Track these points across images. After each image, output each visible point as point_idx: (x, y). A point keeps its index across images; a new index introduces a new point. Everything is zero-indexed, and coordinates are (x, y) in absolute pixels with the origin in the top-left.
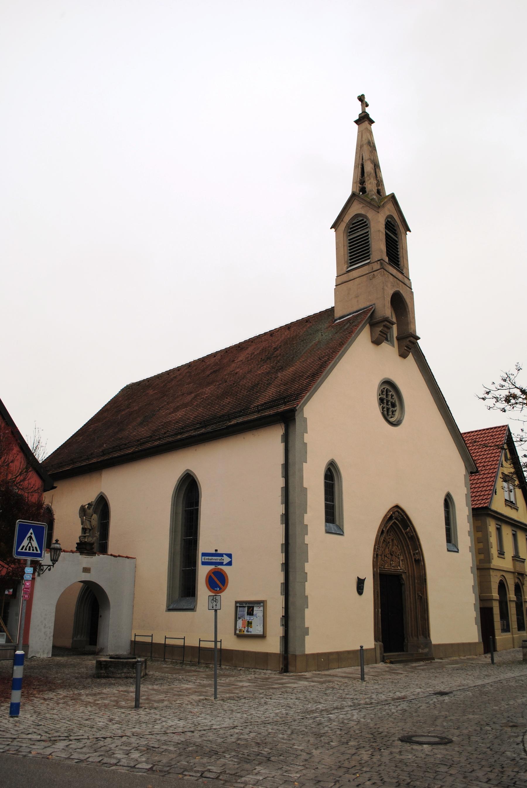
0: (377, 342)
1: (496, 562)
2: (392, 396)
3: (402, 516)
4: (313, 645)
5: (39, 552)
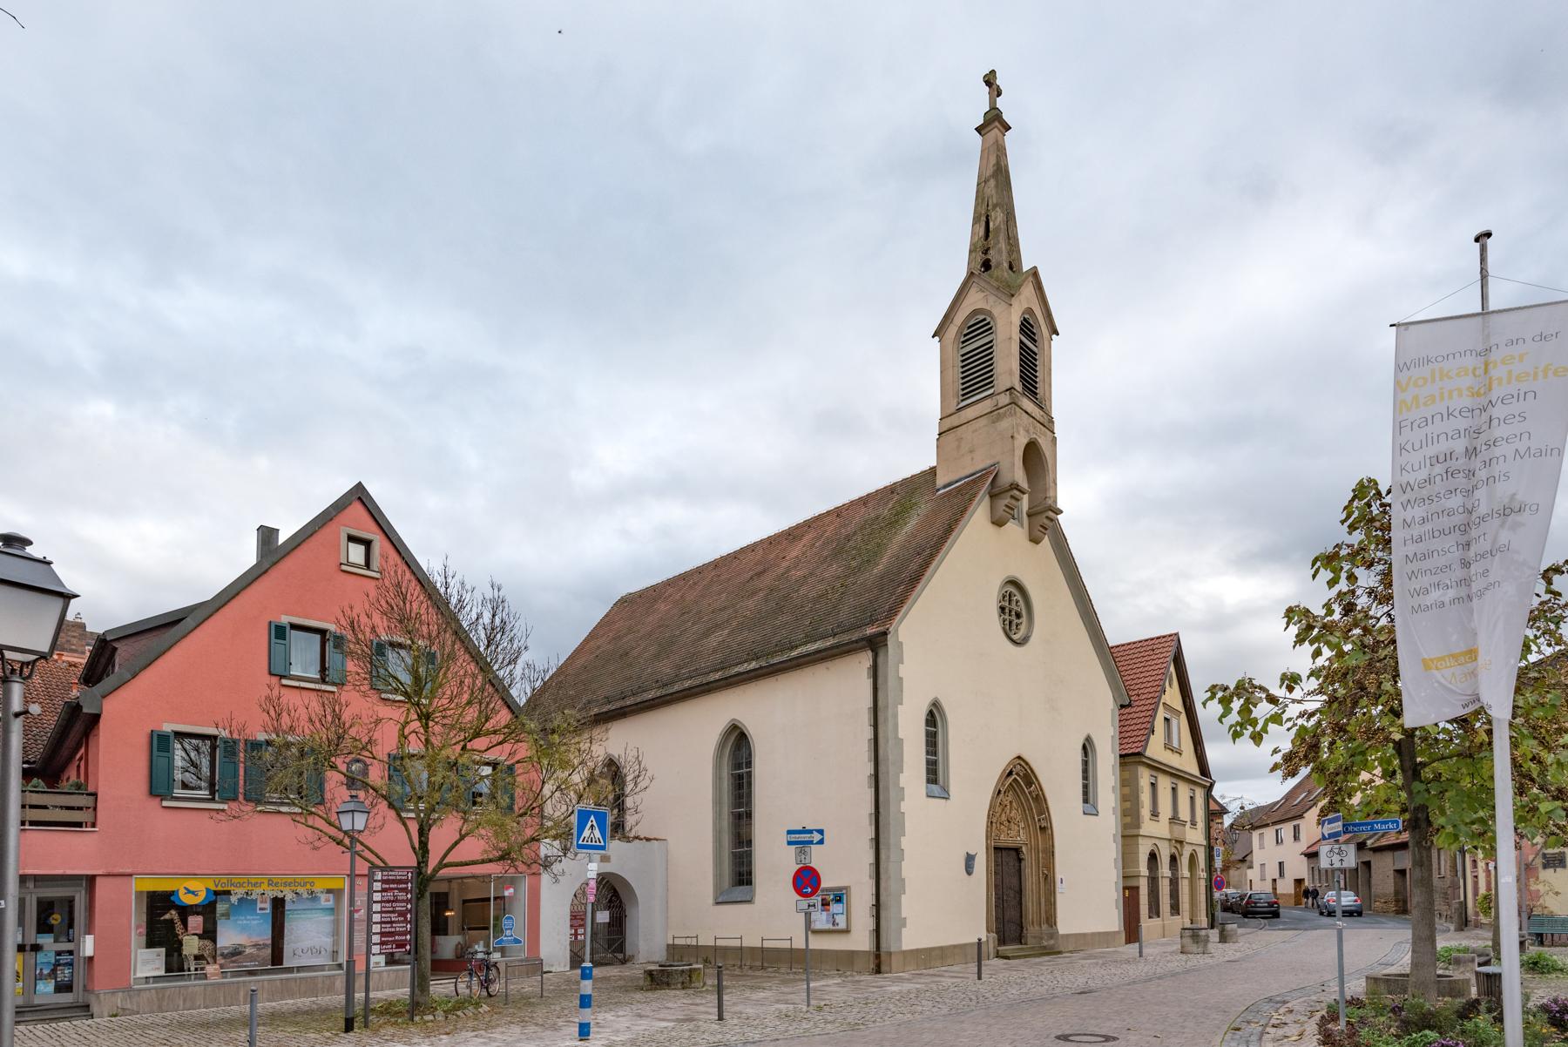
0: (998, 523)
1: (1148, 827)
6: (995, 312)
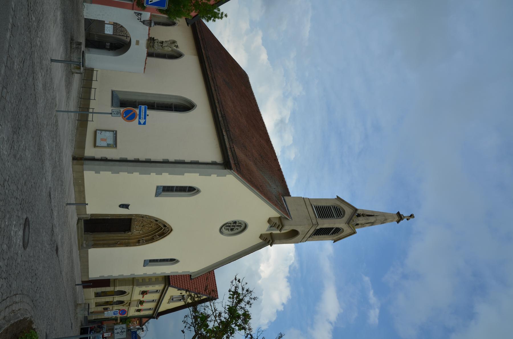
1: (138, 290)
4: (89, 176)
5: (149, 3)
6: (344, 218)
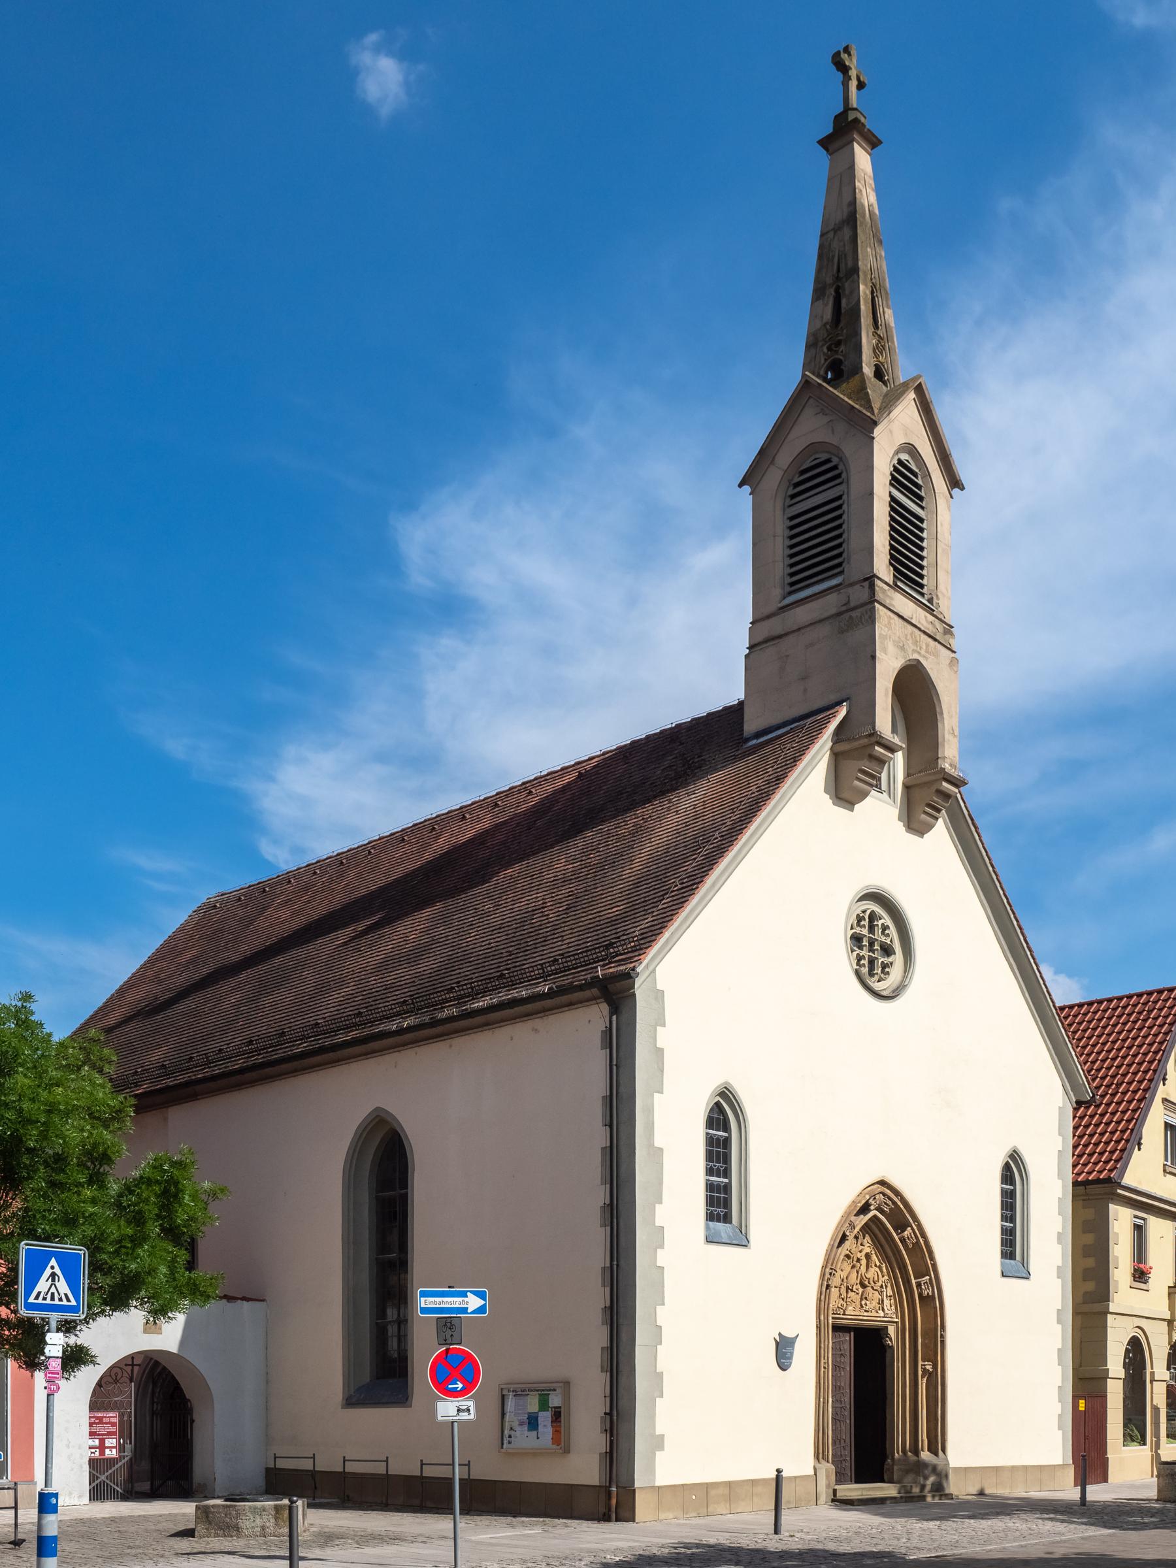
2: (885, 928)
3: (894, 1203)
5: (73, 1303)
